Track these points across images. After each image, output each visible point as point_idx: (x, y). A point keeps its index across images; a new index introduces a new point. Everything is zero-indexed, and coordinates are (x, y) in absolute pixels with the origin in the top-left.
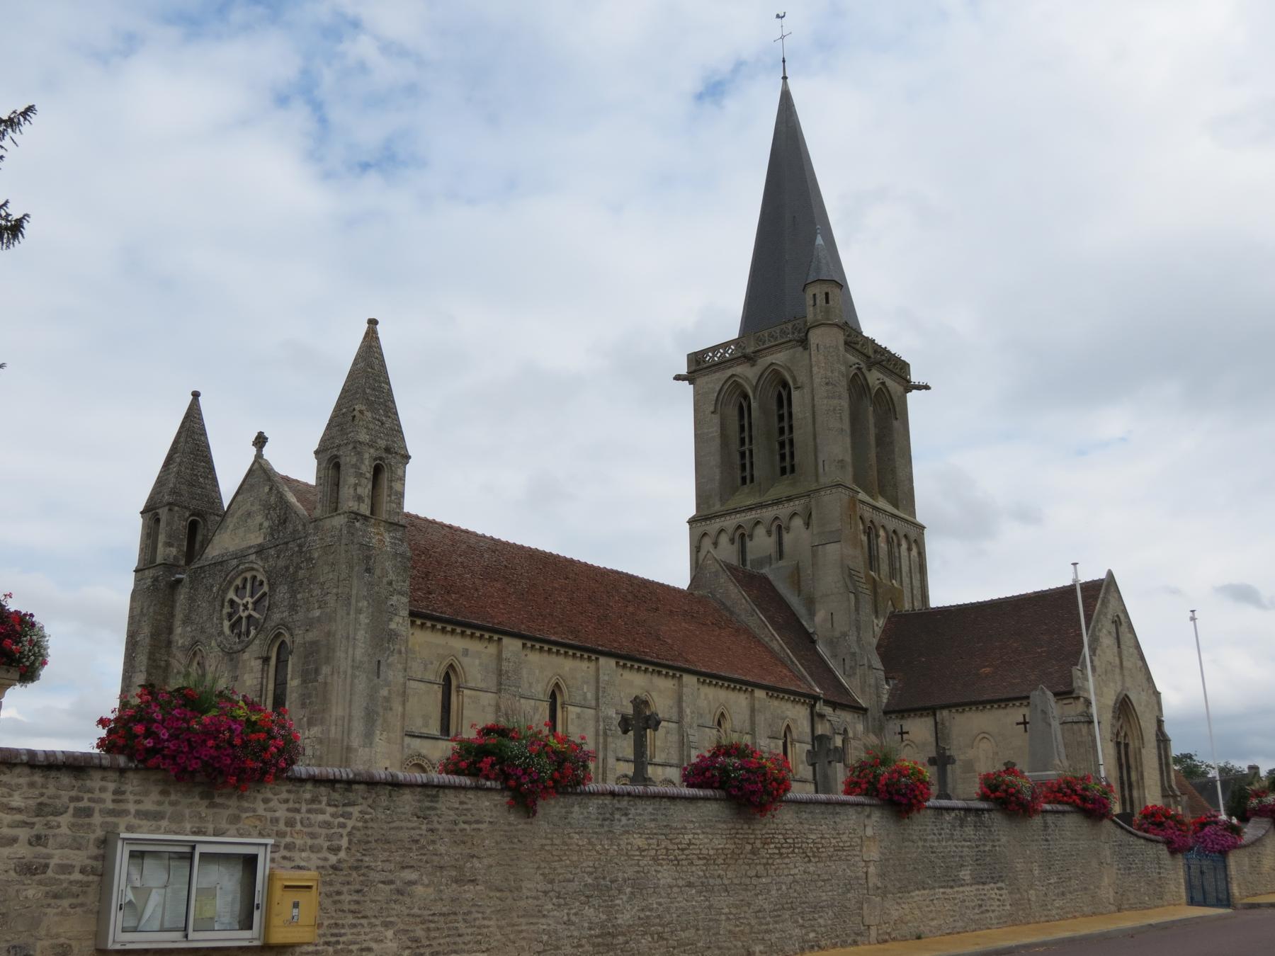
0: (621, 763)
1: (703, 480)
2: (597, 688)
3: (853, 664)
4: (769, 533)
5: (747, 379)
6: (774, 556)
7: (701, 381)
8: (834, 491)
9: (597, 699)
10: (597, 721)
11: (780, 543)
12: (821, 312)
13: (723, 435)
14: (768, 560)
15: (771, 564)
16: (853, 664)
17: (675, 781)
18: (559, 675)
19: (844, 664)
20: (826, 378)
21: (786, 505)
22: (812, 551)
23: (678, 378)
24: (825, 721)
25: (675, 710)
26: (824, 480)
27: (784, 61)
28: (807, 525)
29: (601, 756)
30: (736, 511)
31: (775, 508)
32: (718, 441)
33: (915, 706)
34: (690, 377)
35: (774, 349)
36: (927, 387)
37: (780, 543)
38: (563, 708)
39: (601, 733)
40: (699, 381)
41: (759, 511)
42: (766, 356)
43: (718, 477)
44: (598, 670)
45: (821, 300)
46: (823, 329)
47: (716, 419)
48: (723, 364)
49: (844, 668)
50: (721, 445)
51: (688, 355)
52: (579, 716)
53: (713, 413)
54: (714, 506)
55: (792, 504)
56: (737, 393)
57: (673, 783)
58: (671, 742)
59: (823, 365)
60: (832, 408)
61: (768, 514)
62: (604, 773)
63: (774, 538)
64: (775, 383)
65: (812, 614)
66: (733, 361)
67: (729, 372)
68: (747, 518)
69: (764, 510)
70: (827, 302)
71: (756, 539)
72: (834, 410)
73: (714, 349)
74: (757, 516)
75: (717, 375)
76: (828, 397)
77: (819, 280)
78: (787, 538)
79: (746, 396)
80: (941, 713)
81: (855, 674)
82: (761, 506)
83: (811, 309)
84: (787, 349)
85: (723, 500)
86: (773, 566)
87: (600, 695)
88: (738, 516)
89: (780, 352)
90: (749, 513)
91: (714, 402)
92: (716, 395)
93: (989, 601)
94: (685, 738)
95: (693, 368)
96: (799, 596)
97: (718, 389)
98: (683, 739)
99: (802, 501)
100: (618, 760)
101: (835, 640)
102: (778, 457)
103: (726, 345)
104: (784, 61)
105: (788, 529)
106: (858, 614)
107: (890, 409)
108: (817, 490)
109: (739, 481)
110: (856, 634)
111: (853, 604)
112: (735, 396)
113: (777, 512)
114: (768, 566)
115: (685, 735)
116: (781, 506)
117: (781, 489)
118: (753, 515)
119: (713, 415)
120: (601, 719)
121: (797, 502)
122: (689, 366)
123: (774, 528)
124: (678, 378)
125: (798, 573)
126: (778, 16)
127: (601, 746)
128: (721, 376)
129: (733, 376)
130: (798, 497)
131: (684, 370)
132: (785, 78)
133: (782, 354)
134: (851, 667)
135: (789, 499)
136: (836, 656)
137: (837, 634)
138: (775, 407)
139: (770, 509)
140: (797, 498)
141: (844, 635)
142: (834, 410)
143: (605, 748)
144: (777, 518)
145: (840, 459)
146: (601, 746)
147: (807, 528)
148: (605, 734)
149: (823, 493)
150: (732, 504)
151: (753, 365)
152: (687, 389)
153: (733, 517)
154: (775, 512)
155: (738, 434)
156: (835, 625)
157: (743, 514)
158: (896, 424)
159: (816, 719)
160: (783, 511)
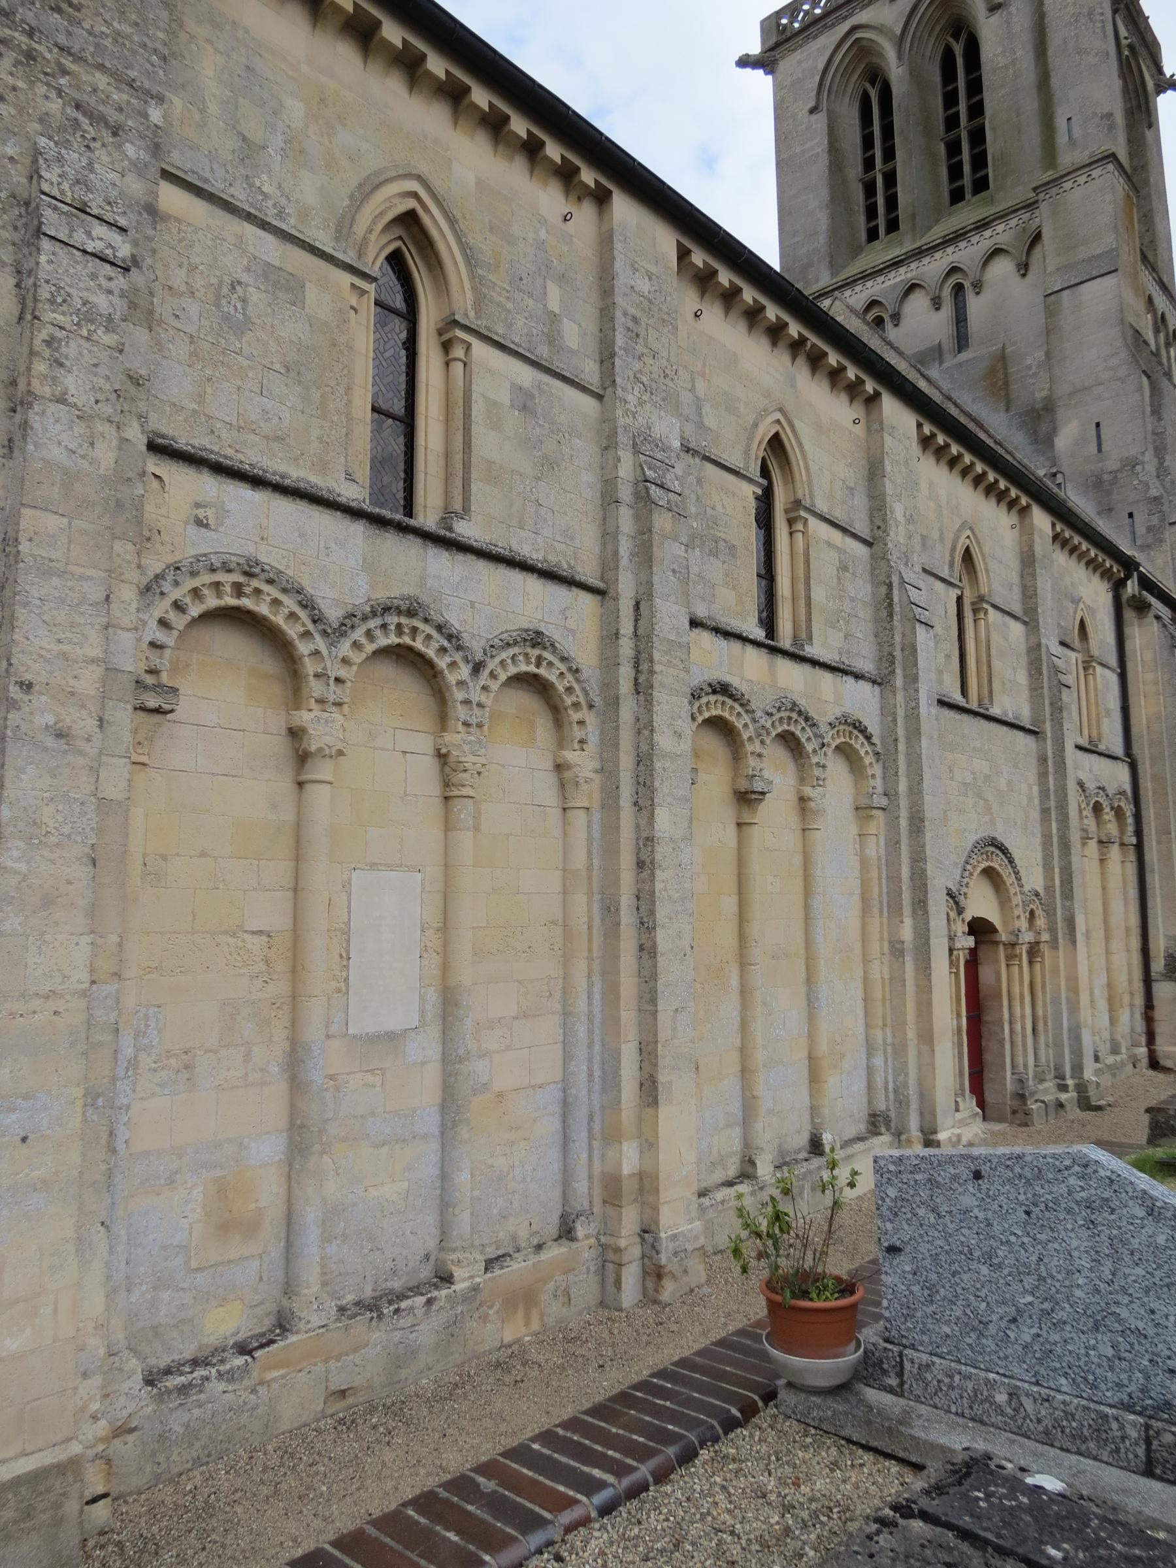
0: (705, 638)
2: (606, 314)
3: (1155, 520)
4: (937, 304)
5: (880, 29)
7: (790, 63)
9: (607, 358)
10: (609, 444)
11: (961, 319)
13: (834, 149)
14: (936, 353)
15: (941, 363)
16: (1155, 520)
17: (866, 722)
18: (419, 178)
22: (1047, 307)
23: (745, 62)
25: (860, 502)
29: (626, 587)
30: (865, 276)
31: (950, 250)
32: (824, 161)
34: (763, 62)
37: (961, 319)
38: (446, 346)
39: (625, 493)
40: (783, 66)
41: (913, 266)
43: (824, 227)
44: (606, 242)
47: (820, 122)
50: (830, 170)
52: (525, 403)
53: (812, 111)
54: (817, 281)
55: (987, 233)
57: (863, 731)
60: (1085, 10)
61: (933, 267)
62: (641, 661)
63: (947, 310)
65: (1044, 441)
67: (845, 27)
68: (888, 284)
69: (926, 260)
71: (907, 322)
72: (1090, 14)
74: (909, 275)
78: (975, 305)
82: (919, 253)
85: (834, 268)
86: (946, 365)
87: (620, 340)
88: (869, 284)
90: (893, 274)
91: (814, 93)
92: (817, 78)
94: (896, 592)
96: (1007, 410)
97: (821, 66)
98: (889, 596)
99: (1013, 223)
100: (695, 623)
102: (944, 172)
105: (978, 287)
106: (1160, 419)
107: (1139, 107)
108: (1056, 182)
109: (863, 235)
110: (1155, 461)
113: (955, 257)
115: (895, 580)
116: (962, 244)
117: (966, 214)
118: (902, 275)
119: (814, 117)
120: (622, 438)
121: (1000, 228)
122: (763, 42)
123: (947, 292)
124: (745, 62)
125: (1005, 368)
127: (625, 548)
129: (855, 28)
130: (1003, 216)
131: (755, 48)
135: (982, 225)
136: (1110, 510)
137: (1112, 464)
138: (937, 79)
139: (938, 255)
141: (1132, 464)
142: (1090, 14)
143: (645, 556)
145: (1106, 111)
146: (625, 548)
147: (1024, 275)
148: (644, 501)
149: (1067, 185)
150: (864, 262)
152: (761, 83)
153: (858, 288)
154: (951, 259)
155: (859, 151)
157: (880, 279)
158: (1149, 134)
159: (1129, 615)
160: (967, 254)
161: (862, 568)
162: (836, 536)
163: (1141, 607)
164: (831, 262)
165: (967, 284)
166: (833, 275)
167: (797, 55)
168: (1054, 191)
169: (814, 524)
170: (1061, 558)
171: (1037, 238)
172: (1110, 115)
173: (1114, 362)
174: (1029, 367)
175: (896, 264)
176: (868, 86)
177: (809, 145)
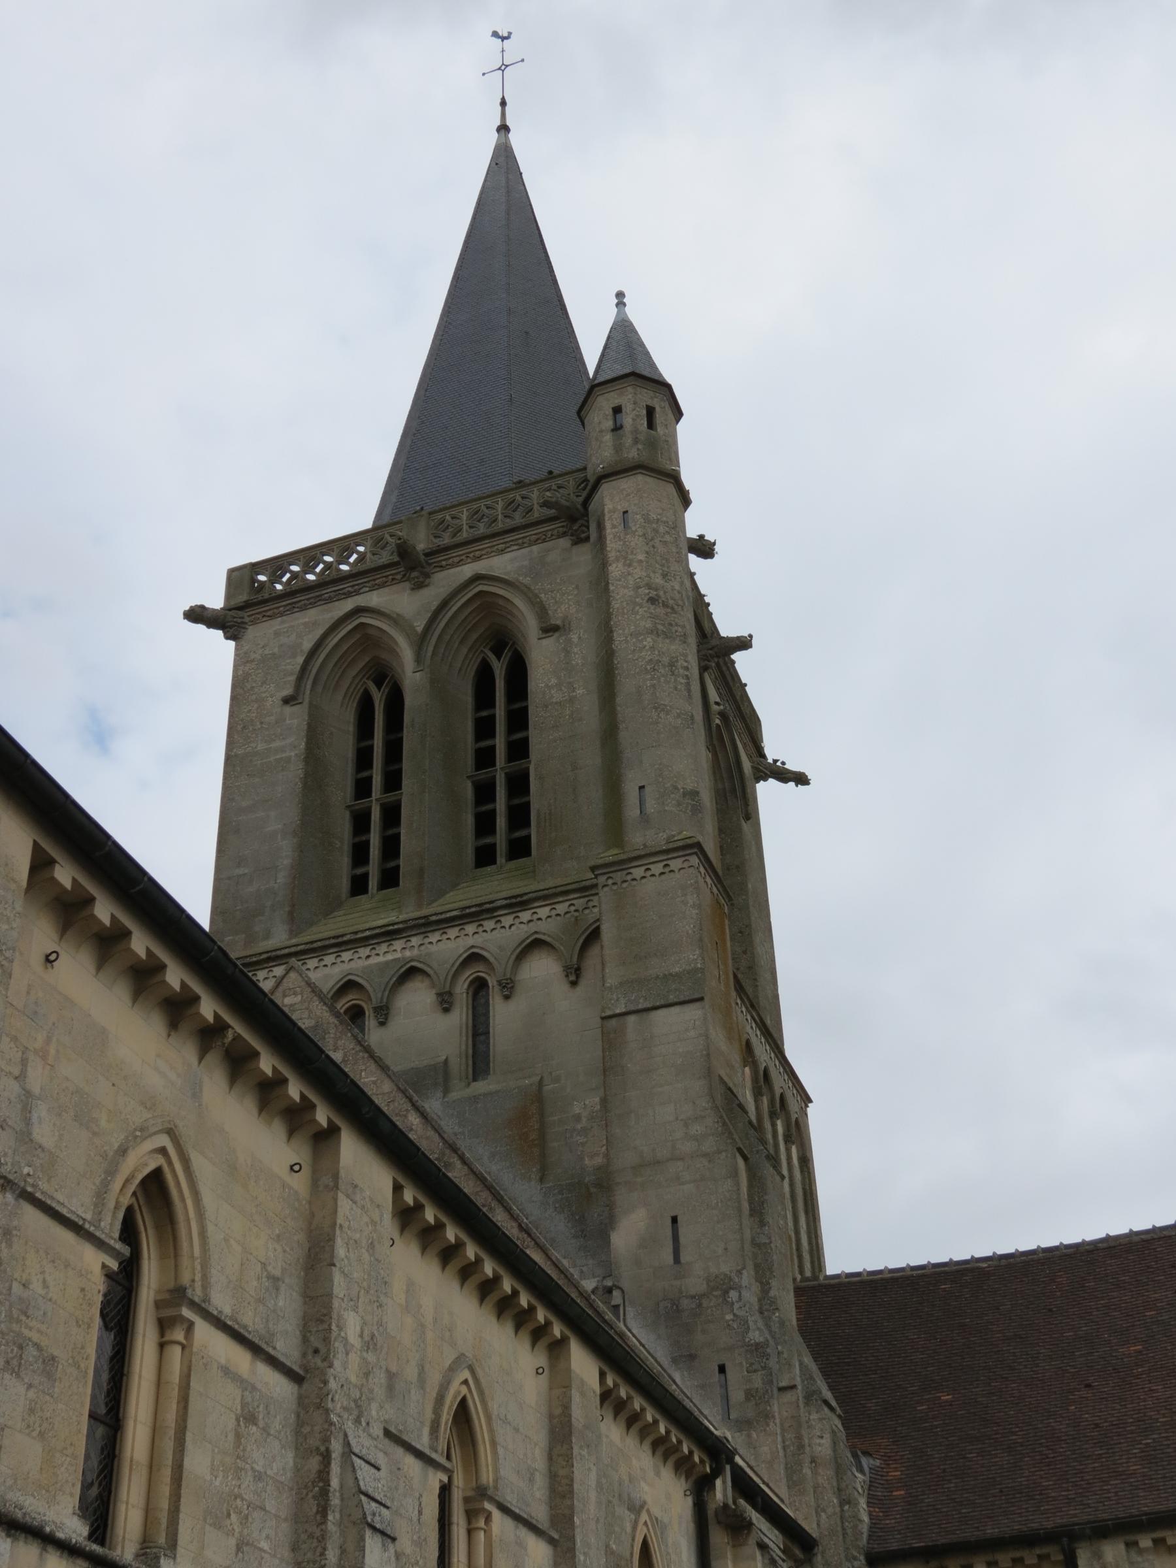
1: (241, 871)
3: (757, 1381)
4: (445, 1003)
5: (395, 620)
6: (456, 1065)
7: (262, 633)
8: (675, 864)
11: (479, 1029)
12: (636, 441)
15: (446, 1091)
19: (725, 1386)
20: (648, 585)
21: (507, 921)
23: (197, 615)
24: (751, 1548)
25: (288, 1302)
26: (638, 839)
27: (503, 103)
28: (574, 974)
30: (341, 944)
31: (470, 928)
32: (296, 770)
33: (991, 1531)
35: (486, 544)
36: (801, 779)
37: (479, 1029)
40: (252, 632)
41: (415, 941)
42: (458, 564)
45: (633, 419)
46: (640, 477)
47: (296, 718)
48: (332, 584)
49: (726, 1398)
51: (231, 572)
53: (287, 701)
54: (267, 935)
55: (525, 916)
56: (361, 664)
58: (259, 1477)
59: (641, 557)
60: (666, 660)
63: (460, 1015)
64: (475, 636)
66: (364, 576)
67: (348, 605)
68: (374, 960)
70: (651, 425)
72: (672, 664)
73: (309, 556)
74: (408, 953)
75: (312, 614)
76: (654, 631)
77: (633, 374)
79: (383, 674)
80: (1098, 1556)
81: (767, 1416)
82: (425, 925)
83: (608, 437)
84: (522, 546)
85: (295, 923)
86: (454, 1095)
88: (346, 956)
89: (502, 552)
90: (384, 947)
91: (293, 678)
92: (300, 660)
93: (1101, 1240)
94: (335, 1468)
95: (243, 598)
96: (541, 1180)
97: (307, 645)
99: (561, 908)
101: (685, 1303)
103: (342, 545)
104: (503, 103)
105: (508, 989)
106: (762, 1224)
107: (734, 790)
108: (622, 864)
109: (345, 884)
111: (745, 1190)
112: (353, 672)
113: (478, 940)
114: (439, 1094)
115: (336, 1447)
116: (489, 924)
119: (288, 710)
121: (544, 912)
122: (229, 596)
123: (461, 988)
124: (197, 615)
126: (495, 34)
128: (319, 617)
130: (548, 897)
131: (216, 600)
132: (503, 128)
133: (507, 557)
134: (749, 1395)
135: (518, 904)
136: (692, 1357)
137: (695, 1284)
139: (453, 933)
140: (545, 898)
141: (723, 1287)
142: (672, 664)
144: (474, 958)
145: (689, 787)
147: (574, 984)
149: (638, 872)
151: (419, 586)
153: (329, 959)
156: (685, 1257)
157: (364, 951)
158: (746, 826)
159: (718, 1538)
161: (280, 1422)
162: (241, 1359)
163: (738, 1528)
164: (291, 913)
165: (492, 982)
166: (293, 933)
167: (276, 624)
168: (618, 877)
169: (204, 1332)
170: (613, 1432)
171: (594, 935)
172: (694, 794)
173: (697, 1129)
174: (578, 1118)
175: (389, 934)
176: (373, 688)
177: (277, 744)
